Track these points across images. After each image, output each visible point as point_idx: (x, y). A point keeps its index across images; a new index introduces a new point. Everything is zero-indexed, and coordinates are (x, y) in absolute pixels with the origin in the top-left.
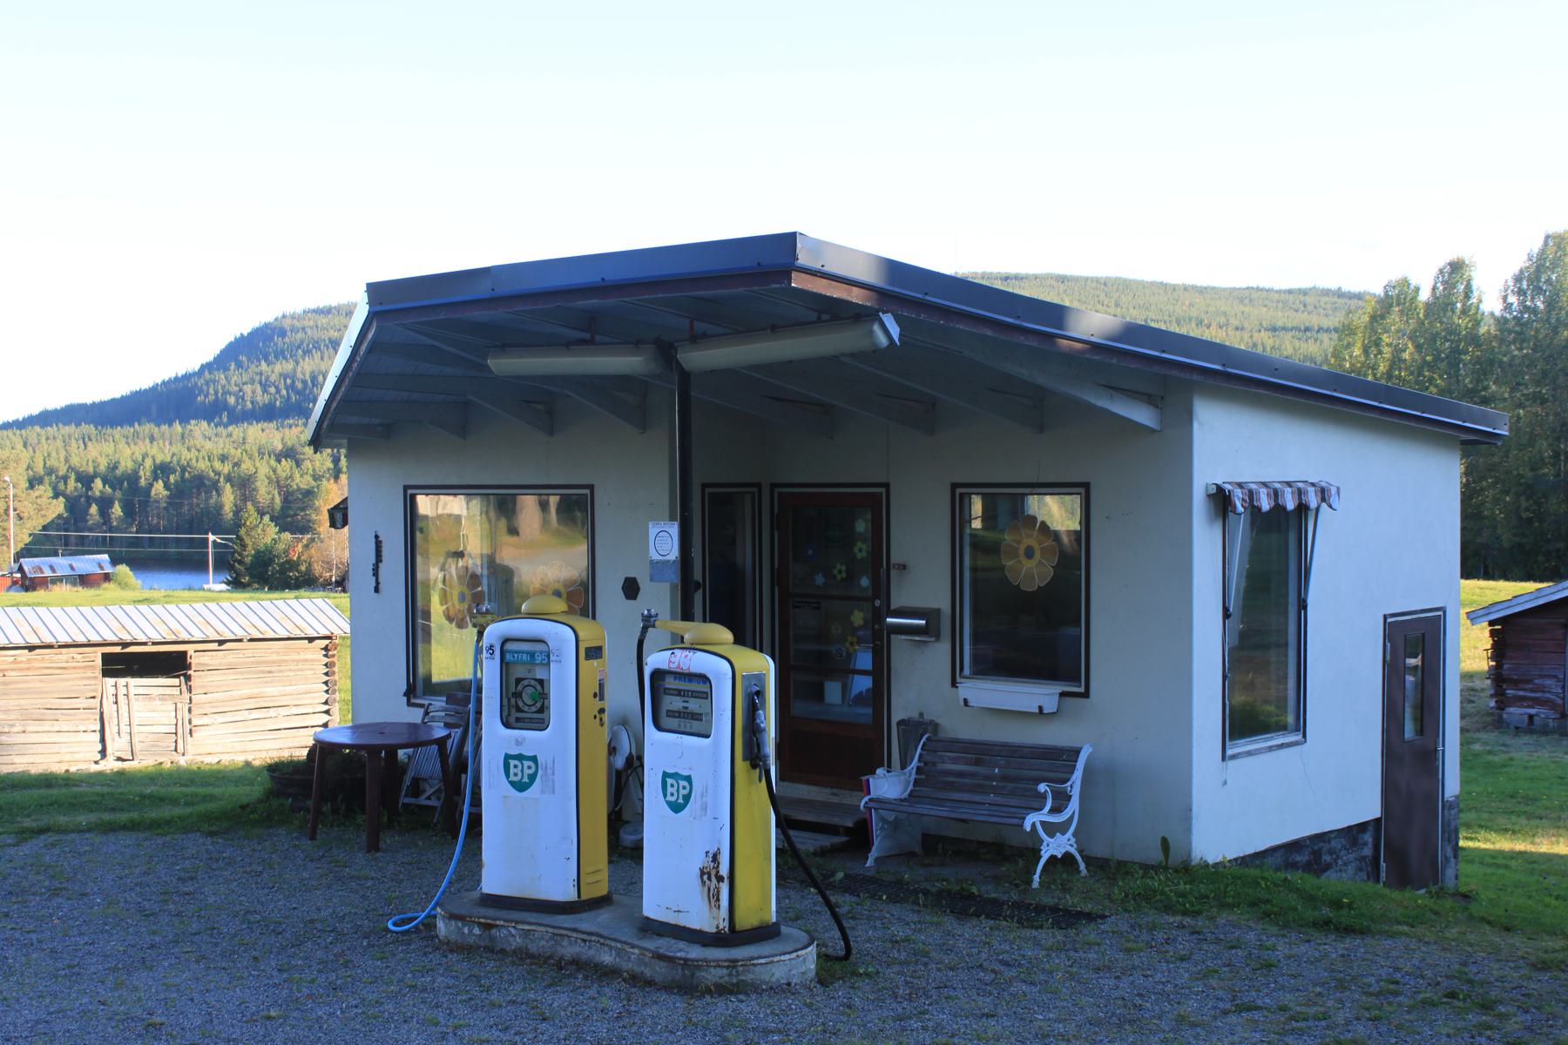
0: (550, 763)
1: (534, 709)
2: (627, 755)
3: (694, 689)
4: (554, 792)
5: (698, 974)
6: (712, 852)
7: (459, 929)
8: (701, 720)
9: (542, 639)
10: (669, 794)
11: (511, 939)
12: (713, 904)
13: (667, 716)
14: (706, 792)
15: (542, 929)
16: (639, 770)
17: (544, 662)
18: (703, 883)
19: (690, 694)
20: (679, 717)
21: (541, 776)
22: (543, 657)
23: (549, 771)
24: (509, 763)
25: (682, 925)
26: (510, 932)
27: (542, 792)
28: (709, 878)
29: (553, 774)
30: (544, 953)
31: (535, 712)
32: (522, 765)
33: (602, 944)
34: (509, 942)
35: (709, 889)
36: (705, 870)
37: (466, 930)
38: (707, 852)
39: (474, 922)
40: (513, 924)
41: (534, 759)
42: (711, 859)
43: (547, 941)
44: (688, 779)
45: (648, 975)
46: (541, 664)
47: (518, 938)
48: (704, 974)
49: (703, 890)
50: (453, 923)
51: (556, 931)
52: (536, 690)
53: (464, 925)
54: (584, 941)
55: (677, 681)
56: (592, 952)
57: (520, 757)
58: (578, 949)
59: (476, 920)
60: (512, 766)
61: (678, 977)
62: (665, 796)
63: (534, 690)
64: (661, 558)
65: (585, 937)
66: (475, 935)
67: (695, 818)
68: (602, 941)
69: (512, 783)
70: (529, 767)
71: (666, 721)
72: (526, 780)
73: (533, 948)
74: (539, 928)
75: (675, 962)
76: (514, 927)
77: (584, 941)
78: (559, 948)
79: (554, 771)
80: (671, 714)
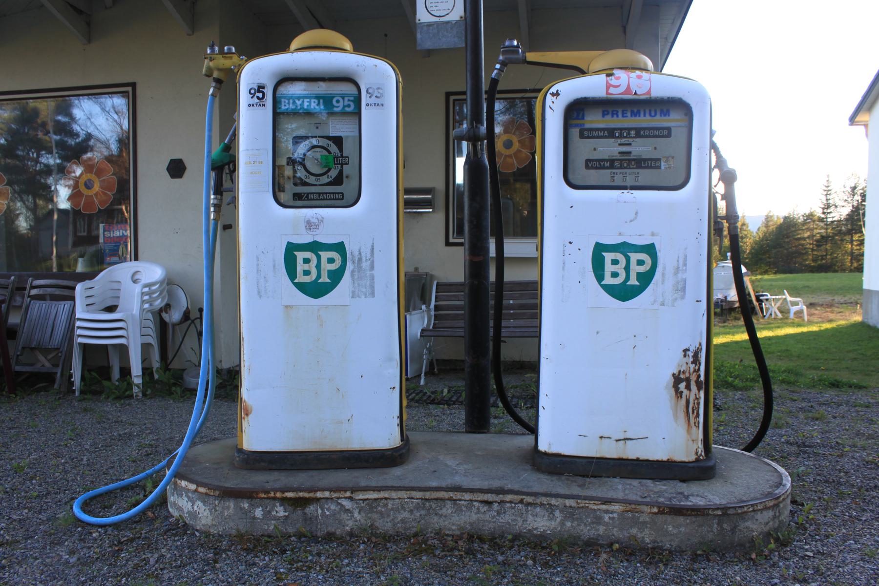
0: (366, 252)
1: (325, 179)
2: (184, 309)
3: (644, 125)
4: (373, 294)
5: (742, 525)
6: (692, 349)
7: (245, 512)
8: (659, 167)
9: (352, 77)
10: (607, 275)
11: (344, 516)
12: (692, 421)
13: (587, 167)
14: (685, 265)
15: (403, 494)
16: (198, 322)
17: (348, 109)
18: (679, 394)
19: (633, 133)
20: (612, 167)
21: (353, 272)
22: (346, 103)
23: (365, 265)
24: (295, 257)
25: (634, 457)
26: (342, 506)
27: (354, 295)
28: (688, 387)
29: (372, 267)
30: (405, 529)
31: (328, 184)
32: (319, 258)
33: (529, 504)
34: (340, 522)
35: (688, 402)
36: (682, 376)
37: (259, 513)
38: (685, 351)
39: (275, 498)
40: (348, 494)
41: (340, 248)
42: (691, 360)
43: (411, 511)
44: (650, 250)
45: (647, 540)
46: (344, 114)
47: (356, 515)
48: (749, 524)
49: (676, 405)
50: (231, 504)
51: (428, 495)
52: (329, 152)
53: (253, 506)
54: (488, 503)
55: (608, 117)
56: (507, 518)
57: (315, 247)
58: (474, 517)
59: (278, 495)
60: (300, 261)
61: (710, 536)
62: (599, 277)
63: (325, 153)
64: (437, 19)
65: (489, 497)
66: (276, 518)
67: (663, 304)
68: (529, 499)
69: (301, 287)
70: (640, 263)
71: (580, 173)
72: (325, 279)
73: (384, 525)
74: (394, 495)
75: (708, 515)
76: (350, 498)
77: (488, 503)
78: (436, 519)
79: (373, 263)
80: (591, 164)
